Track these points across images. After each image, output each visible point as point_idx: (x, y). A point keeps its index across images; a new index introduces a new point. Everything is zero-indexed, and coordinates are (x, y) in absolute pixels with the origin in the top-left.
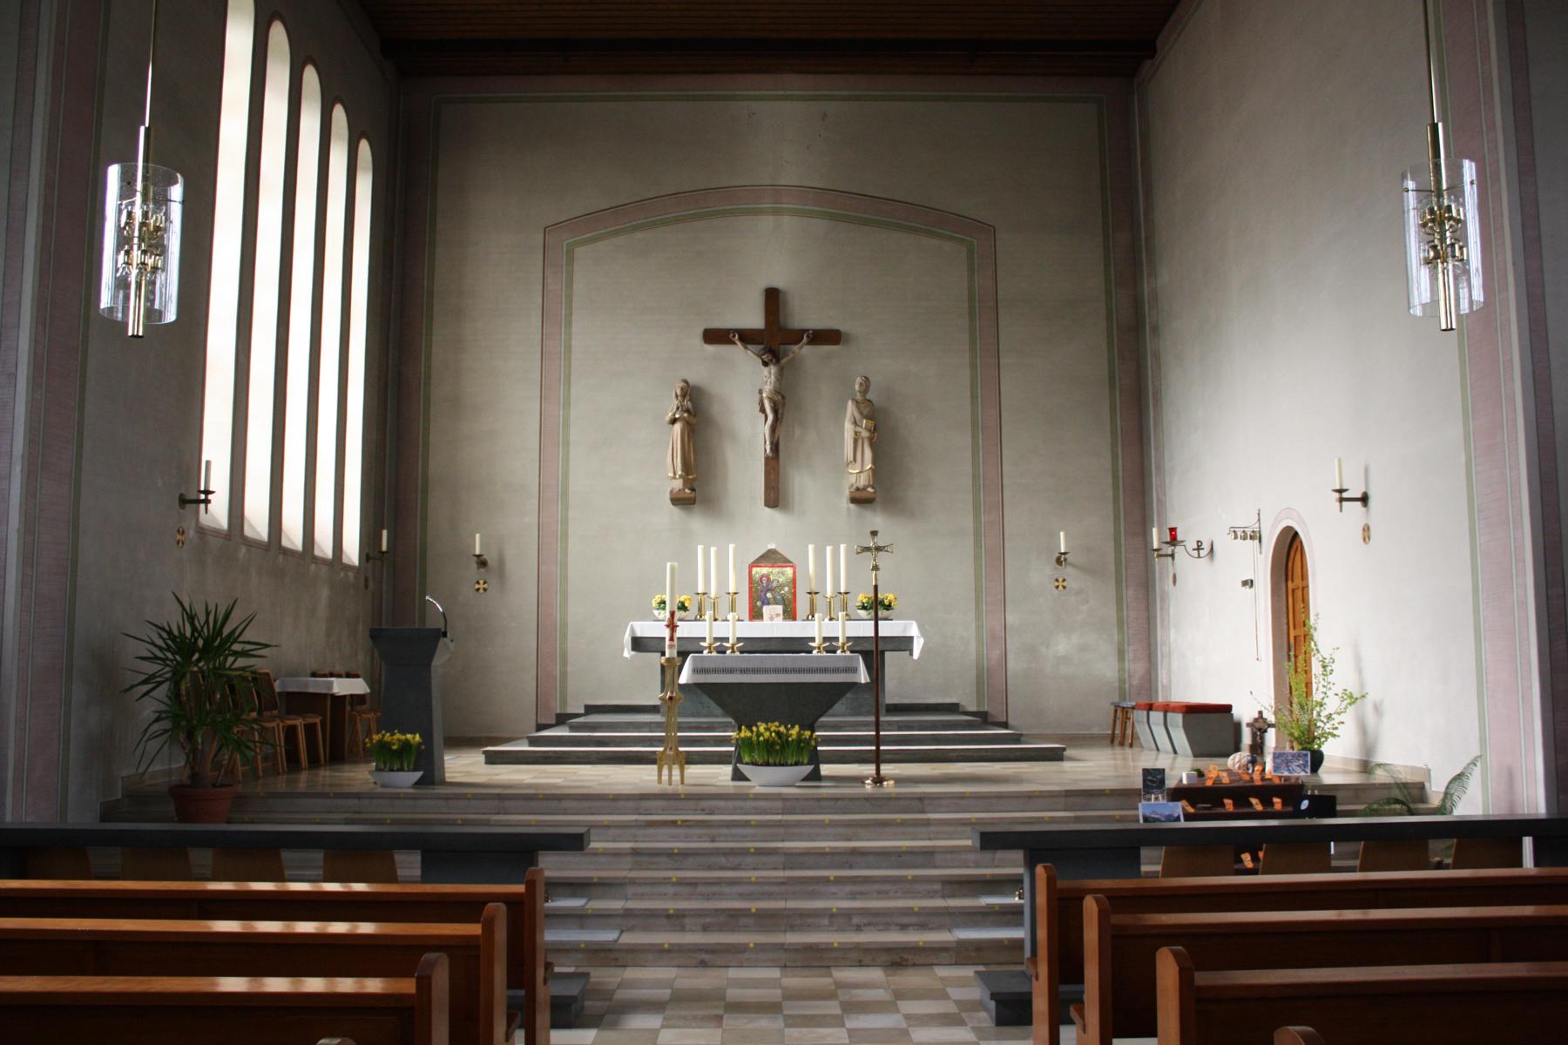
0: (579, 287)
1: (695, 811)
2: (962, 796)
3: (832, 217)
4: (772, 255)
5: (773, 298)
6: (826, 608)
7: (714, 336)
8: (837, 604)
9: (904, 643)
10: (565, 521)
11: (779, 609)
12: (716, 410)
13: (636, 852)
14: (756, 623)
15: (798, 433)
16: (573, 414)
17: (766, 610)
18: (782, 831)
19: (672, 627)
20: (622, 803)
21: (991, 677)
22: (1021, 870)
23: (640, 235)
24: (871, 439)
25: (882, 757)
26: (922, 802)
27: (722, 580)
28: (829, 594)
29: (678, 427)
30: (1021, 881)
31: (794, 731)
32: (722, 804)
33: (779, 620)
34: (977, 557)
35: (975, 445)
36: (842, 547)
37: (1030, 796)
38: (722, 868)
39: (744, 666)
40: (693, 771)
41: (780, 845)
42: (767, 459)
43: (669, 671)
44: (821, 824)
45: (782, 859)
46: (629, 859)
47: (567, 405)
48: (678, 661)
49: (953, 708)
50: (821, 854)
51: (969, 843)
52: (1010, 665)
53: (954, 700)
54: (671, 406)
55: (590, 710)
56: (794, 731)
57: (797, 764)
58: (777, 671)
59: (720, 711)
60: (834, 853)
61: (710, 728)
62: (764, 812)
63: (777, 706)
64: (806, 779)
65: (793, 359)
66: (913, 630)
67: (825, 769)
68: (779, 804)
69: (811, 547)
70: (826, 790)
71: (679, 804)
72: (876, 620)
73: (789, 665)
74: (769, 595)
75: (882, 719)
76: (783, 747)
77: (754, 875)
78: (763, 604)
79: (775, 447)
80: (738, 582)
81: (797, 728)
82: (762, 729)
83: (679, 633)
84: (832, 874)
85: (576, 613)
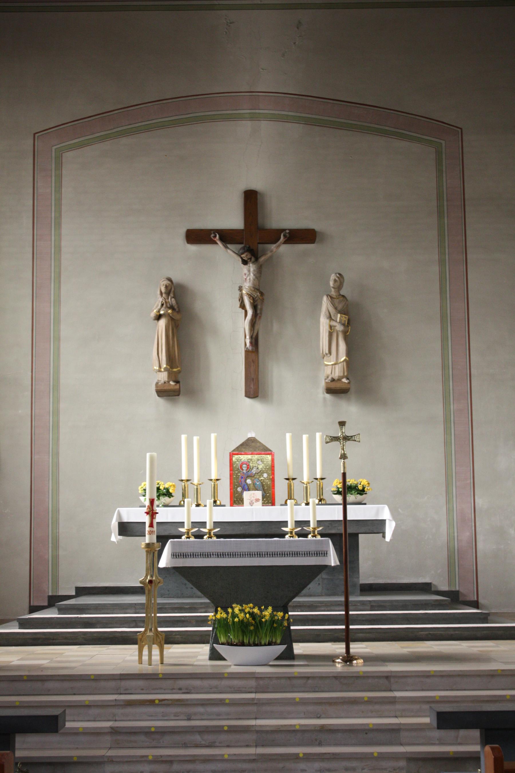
0: (67, 191)
1: (172, 690)
2: (427, 675)
3: (308, 122)
4: (250, 160)
5: (251, 199)
6: (302, 493)
7: (196, 237)
8: (313, 489)
9: (376, 526)
10: (57, 413)
11: (259, 494)
12: (198, 306)
13: (114, 731)
14: (236, 508)
15: (276, 327)
16: (64, 310)
17: (246, 495)
18: (254, 708)
19: (152, 513)
20: (103, 684)
21: (462, 557)
22: (477, 748)
23: (124, 141)
24: (345, 333)
25: (351, 635)
26: (389, 680)
27: (205, 466)
28: (305, 480)
29: (163, 322)
30: (478, 759)
31: (268, 613)
32: (197, 683)
33: (259, 505)
34: (447, 444)
35: (444, 339)
36: (318, 435)
37: (493, 675)
38: (197, 746)
39: (220, 550)
40: (175, 651)
41: (252, 722)
42: (247, 352)
43: (154, 553)
44: (292, 702)
45: (254, 737)
46: (108, 738)
47: (58, 302)
48: (157, 546)
49: (425, 588)
50: (291, 731)
51: (427, 720)
52: (480, 546)
53: (427, 580)
54: (156, 303)
55: (81, 591)
56: (268, 613)
57: (270, 644)
58: (251, 555)
59: (199, 593)
60: (304, 731)
61: (192, 608)
62: (239, 691)
63: (251, 589)
64: (279, 658)
65: (271, 257)
66: (384, 513)
67: (299, 648)
68: (253, 683)
69: (288, 436)
70: (299, 669)
71: (158, 683)
72: (345, 504)
73: (263, 549)
74: (249, 481)
75: (351, 599)
76: (257, 628)
77: (226, 752)
78: (244, 489)
79: (255, 341)
80: (219, 469)
81: (270, 609)
82: (237, 611)
83: (159, 519)
84: (300, 750)
85: (67, 498)
